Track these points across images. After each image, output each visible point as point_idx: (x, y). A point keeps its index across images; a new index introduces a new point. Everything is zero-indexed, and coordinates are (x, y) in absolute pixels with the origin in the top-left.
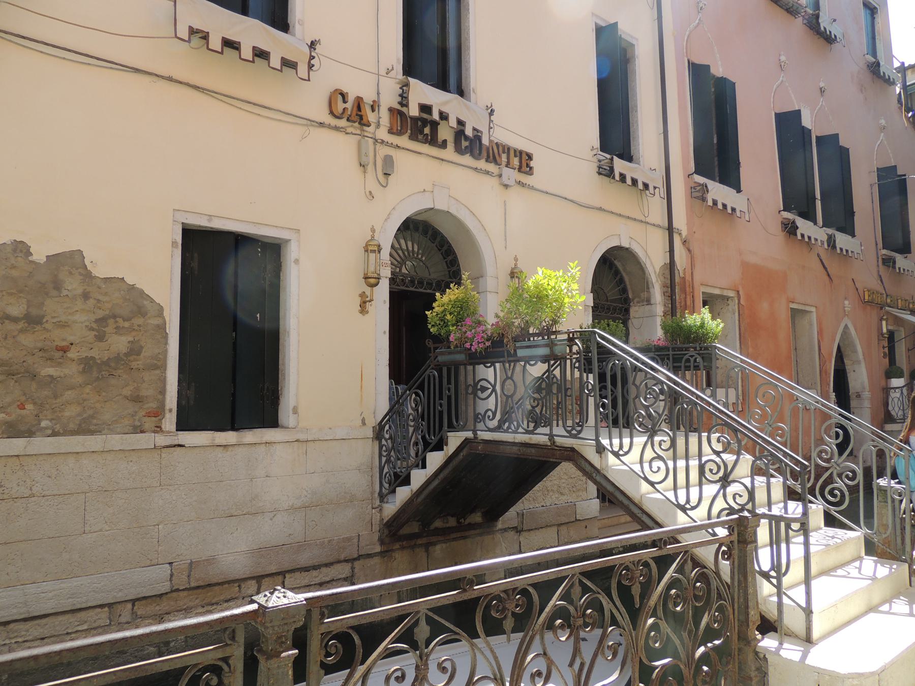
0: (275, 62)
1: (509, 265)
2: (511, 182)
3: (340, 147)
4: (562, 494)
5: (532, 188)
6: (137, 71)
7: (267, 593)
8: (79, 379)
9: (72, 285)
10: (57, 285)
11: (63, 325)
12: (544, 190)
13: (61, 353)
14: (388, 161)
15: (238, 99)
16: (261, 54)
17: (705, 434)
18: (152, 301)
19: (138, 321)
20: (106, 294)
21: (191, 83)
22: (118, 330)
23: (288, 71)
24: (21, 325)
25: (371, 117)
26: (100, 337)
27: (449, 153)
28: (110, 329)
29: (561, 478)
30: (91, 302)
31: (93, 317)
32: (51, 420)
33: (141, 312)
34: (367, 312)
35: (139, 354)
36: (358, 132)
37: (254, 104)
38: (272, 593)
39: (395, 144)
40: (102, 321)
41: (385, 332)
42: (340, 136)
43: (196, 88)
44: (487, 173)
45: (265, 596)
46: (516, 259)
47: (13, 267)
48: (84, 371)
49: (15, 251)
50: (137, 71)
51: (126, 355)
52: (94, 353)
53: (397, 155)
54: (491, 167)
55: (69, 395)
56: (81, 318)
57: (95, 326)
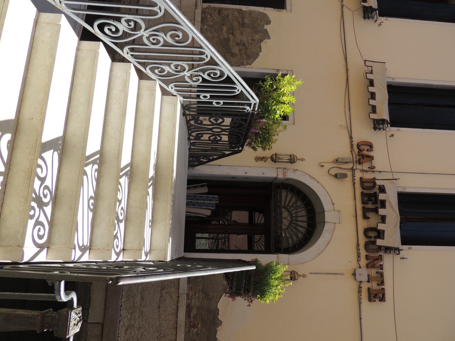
0: (371, 89)
1: (300, 270)
2: (359, 278)
3: (344, 151)
4: (126, 330)
5: (360, 303)
6: (346, 59)
7: (81, 314)
8: (221, 37)
9: (257, 37)
10: (257, 32)
11: (242, 33)
12: (363, 317)
13: (231, 32)
14: (344, 176)
15: (349, 96)
16: (373, 96)
17: (196, 110)
18: (253, 61)
19: (245, 57)
20: (254, 46)
21: (349, 77)
22: (240, 50)
23: (368, 83)
24: (241, 21)
25: (365, 166)
26: (237, 44)
27: (363, 224)
28: (241, 47)
29: (139, 329)
30: (251, 42)
31: (245, 42)
32: (207, 29)
33: (248, 57)
34: (257, 161)
35: (232, 56)
36: (355, 159)
37: (349, 104)
38: (80, 317)
39: (355, 181)
40: (244, 45)
41: (246, 173)
42: (349, 149)
43: (347, 79)
44: (359, 256)
45: (79, 313)
46: (302, 160)
47: (261, 20)
48: (224, 39)
49: (267, 21)
50: (346, 59)
51: (231, 52)
52: (231, 42)
53: (349, 178)
54: (363, 262)
55: (216, 34)
56: (245, 38)
57: (242, 42)
